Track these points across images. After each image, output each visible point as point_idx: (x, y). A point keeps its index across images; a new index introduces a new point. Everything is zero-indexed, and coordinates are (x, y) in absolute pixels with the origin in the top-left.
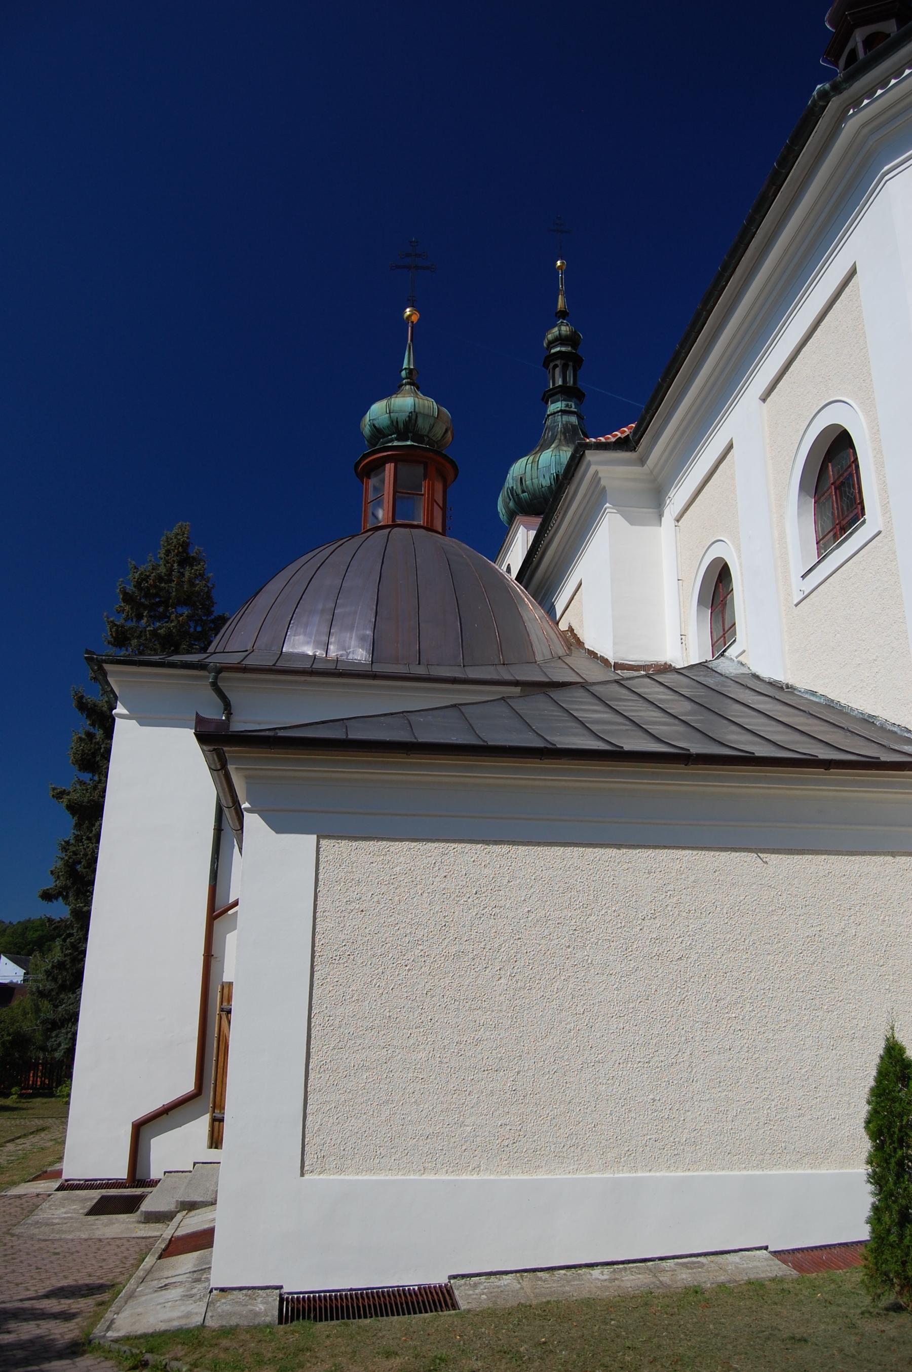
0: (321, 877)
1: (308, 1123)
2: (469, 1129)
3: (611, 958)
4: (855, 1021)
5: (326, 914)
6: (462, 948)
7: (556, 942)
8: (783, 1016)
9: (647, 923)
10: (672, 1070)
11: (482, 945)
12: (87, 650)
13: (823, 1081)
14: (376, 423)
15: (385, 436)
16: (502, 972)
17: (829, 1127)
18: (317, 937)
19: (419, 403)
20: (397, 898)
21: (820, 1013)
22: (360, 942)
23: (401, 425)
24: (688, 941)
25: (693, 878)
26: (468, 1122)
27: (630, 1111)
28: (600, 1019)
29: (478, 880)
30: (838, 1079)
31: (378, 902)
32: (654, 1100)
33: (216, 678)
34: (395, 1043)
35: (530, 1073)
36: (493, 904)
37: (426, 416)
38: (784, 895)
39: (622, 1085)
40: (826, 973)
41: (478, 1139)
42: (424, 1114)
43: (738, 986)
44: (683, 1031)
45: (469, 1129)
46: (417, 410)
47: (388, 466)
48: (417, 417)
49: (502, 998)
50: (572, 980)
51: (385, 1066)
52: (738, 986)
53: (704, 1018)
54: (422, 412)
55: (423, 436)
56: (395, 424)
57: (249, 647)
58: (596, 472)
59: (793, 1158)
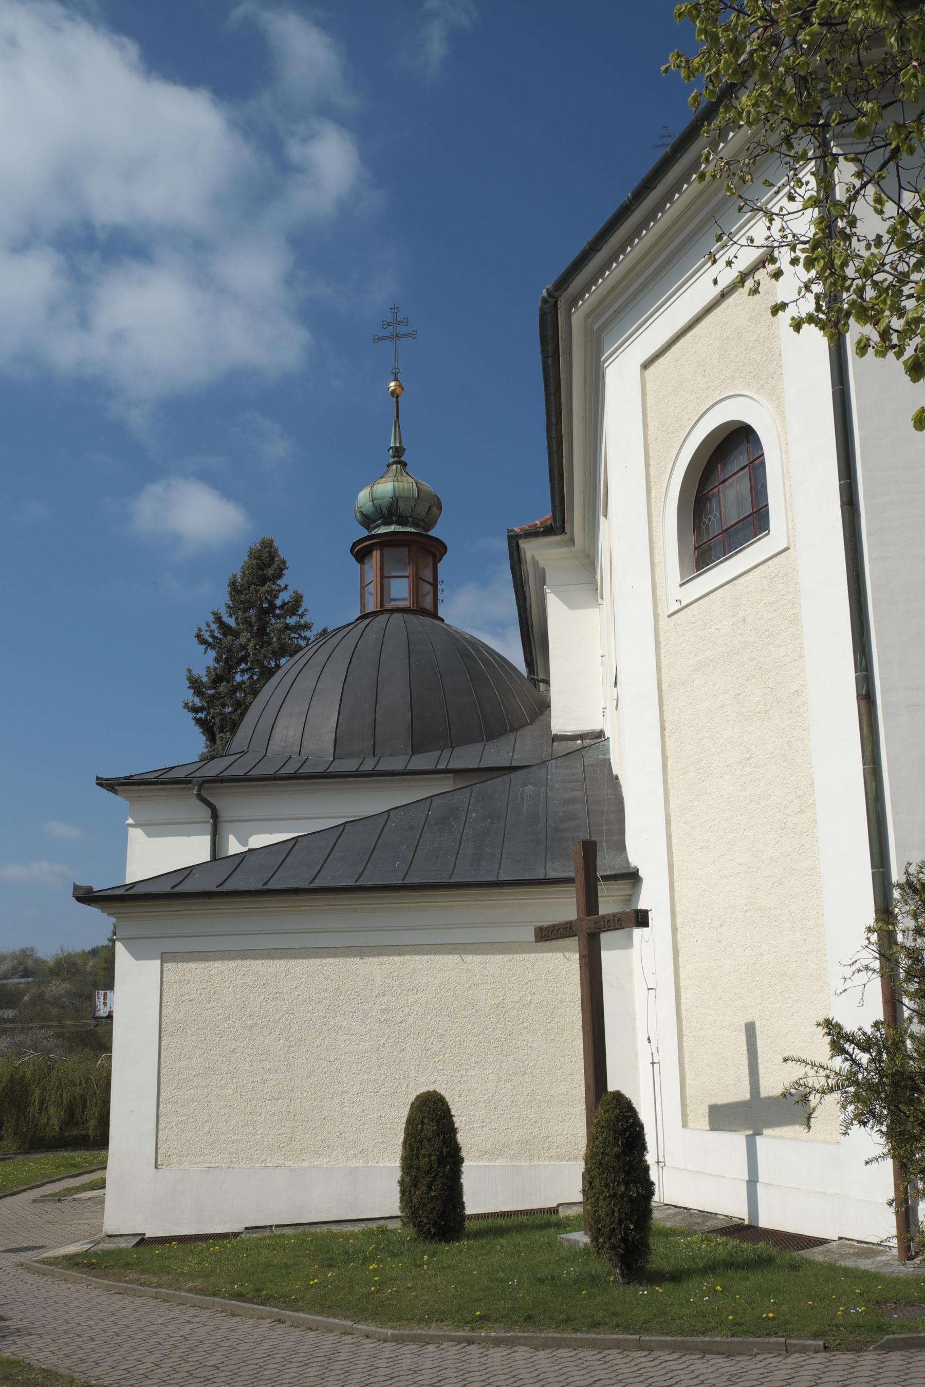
0: (164, 980)
1: (160, 1135)
2: (259, 1137)
3: (354, 1024)
4: (527, 1062)
5: (169, 1003)
6: (255, 1021)
7: (317, 1014)
8: (473, 1059)
9: (378, 999)
10: (393, 1097)
11: (268, 1019)
12: (98, 778)
13: (501, 1103)
14: (363, 510)
15: (374, 521)
16: (281, 1036)
17: (503, 1134)
18: (163, 1019)
19: (399, 487)
20: (212, 991)
21: (501, 1057)
22: (189, 1021)
23: (385, 511)
24: (407, 1010)
25: (412, 967)
26: (258, 1132)
27: (364, 1124)
28: (345, 1064)
29: (265, 976)
30: (512, 1102)
31: (201, 994)
32: (381, 1117)
33: (199, 790)
34: (212, 1084)
35: (299, 1100)
36: (275, 991)
37: (407, 499)
38: (478, 976)
39: (360, 1107)
40: (506, 1029)
41: (265, 1143)
42: (231, 1128)
43: (441, 1039)
44: (402, 1072)
45: (259, 1137)
46: (396, 495)
47: (374, 553)
48: (397, 501)
49: (281, 1053)
50: (327, 1039)
51: (206, 1099)
52: (441, 1039)
53: (416, 1062)
54: (402, 495)
55: (407, 517)
56: (379, 510)
57: (246, 749)
58: (533, 557)
59: (477, 1155)
